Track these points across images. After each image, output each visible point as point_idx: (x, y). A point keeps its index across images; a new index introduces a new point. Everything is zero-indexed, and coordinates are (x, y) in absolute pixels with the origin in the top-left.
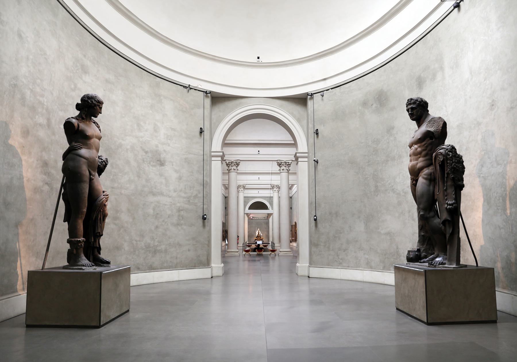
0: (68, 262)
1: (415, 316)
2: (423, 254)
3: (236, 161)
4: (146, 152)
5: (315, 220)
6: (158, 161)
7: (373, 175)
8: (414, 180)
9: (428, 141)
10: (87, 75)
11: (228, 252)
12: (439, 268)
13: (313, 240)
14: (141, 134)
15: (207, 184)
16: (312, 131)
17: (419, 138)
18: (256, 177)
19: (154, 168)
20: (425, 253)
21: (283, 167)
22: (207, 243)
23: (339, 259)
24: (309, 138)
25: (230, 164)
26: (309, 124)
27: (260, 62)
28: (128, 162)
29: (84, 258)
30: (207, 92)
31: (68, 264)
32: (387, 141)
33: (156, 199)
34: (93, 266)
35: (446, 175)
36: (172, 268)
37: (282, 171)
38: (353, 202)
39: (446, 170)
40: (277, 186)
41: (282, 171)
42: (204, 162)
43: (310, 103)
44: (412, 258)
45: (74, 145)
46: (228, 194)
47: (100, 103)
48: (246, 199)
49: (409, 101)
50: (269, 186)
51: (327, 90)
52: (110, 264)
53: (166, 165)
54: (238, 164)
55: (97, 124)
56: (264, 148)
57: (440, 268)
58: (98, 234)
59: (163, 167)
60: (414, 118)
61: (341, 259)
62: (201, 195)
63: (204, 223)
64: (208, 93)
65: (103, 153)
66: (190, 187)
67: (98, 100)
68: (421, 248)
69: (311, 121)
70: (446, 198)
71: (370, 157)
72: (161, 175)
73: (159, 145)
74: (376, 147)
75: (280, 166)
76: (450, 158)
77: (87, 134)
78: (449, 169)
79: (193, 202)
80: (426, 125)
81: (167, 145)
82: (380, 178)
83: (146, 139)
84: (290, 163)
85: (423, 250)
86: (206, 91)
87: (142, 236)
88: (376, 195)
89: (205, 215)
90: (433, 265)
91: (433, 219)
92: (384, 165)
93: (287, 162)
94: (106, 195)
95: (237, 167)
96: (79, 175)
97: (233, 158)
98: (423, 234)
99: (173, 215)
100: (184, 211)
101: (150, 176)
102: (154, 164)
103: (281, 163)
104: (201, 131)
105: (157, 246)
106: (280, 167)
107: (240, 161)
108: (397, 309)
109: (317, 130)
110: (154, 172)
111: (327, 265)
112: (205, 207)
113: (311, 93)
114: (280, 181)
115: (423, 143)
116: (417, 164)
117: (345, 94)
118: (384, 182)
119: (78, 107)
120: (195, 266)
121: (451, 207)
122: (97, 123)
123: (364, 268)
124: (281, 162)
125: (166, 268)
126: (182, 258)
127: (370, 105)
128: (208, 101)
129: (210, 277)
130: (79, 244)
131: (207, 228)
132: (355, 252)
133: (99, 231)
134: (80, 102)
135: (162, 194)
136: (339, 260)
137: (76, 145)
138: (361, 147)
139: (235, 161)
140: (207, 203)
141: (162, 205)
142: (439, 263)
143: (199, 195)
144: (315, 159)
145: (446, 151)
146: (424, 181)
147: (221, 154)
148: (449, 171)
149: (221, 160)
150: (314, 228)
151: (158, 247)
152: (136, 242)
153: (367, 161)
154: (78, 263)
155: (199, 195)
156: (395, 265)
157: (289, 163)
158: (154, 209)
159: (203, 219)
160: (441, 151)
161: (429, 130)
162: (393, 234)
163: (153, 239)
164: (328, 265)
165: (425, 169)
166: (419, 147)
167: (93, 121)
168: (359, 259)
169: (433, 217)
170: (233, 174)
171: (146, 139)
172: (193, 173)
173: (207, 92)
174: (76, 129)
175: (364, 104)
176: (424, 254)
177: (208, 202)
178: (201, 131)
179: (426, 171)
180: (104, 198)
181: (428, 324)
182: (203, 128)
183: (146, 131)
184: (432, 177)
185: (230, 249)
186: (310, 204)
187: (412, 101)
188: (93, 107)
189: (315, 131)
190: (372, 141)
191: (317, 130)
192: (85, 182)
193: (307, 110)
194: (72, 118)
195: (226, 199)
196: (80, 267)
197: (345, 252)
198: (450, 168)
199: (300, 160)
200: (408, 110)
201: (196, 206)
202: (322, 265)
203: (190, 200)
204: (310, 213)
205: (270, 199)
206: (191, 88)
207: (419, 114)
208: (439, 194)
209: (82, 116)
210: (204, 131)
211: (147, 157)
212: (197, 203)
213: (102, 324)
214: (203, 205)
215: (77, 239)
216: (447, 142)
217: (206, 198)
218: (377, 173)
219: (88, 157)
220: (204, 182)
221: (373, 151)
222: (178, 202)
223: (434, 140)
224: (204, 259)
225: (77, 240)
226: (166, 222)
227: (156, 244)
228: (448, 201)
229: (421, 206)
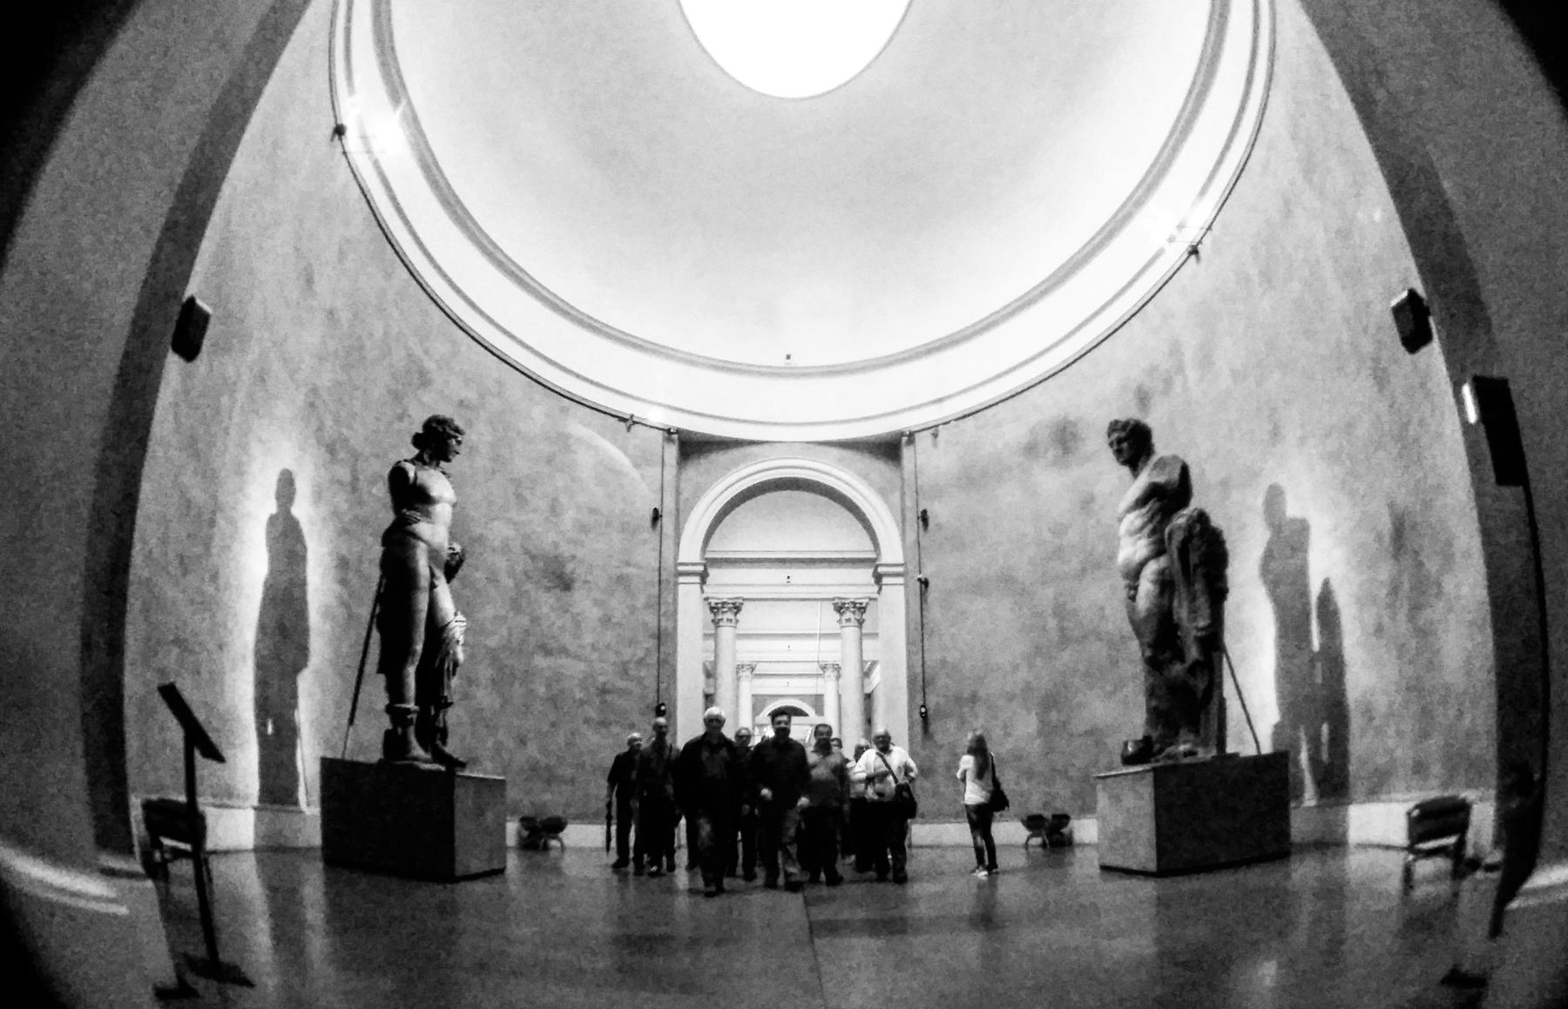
2: (1157, 747)
4: (533, 558)
9: (1152, 505)
16: (912, 516)
18: (781, 644)
21: (848, 615)
28: (493, 579)
37: (844, 623)
43: (907, 452)
50: (814, 669)
54: (737, 609)
62: (653, 660)
84: (864, 605)
87: (523, 742)
95: (736, 614)
97: (726, 594)
104: (656, 517)
106: (841, 614)
112: (663, 686)
116: (1136, 552)
128: (672, 452)
134: (421, 432)
135: (564, 651)
144: (920, 576)
147: (701, 568)
158: (548, 686)
163: (544, 750)
169: (1171, 661)
170: (726, 632)
178: (656, 517)
183: (535, 511)
186: (911, 680)
187: (1119, 426)
194: (406, 461)
199: (885, 580)
200: (1111, 444)
204: (911, 699)
206: (635, 423)
208: (1182, 612)
216: (1195, 503)
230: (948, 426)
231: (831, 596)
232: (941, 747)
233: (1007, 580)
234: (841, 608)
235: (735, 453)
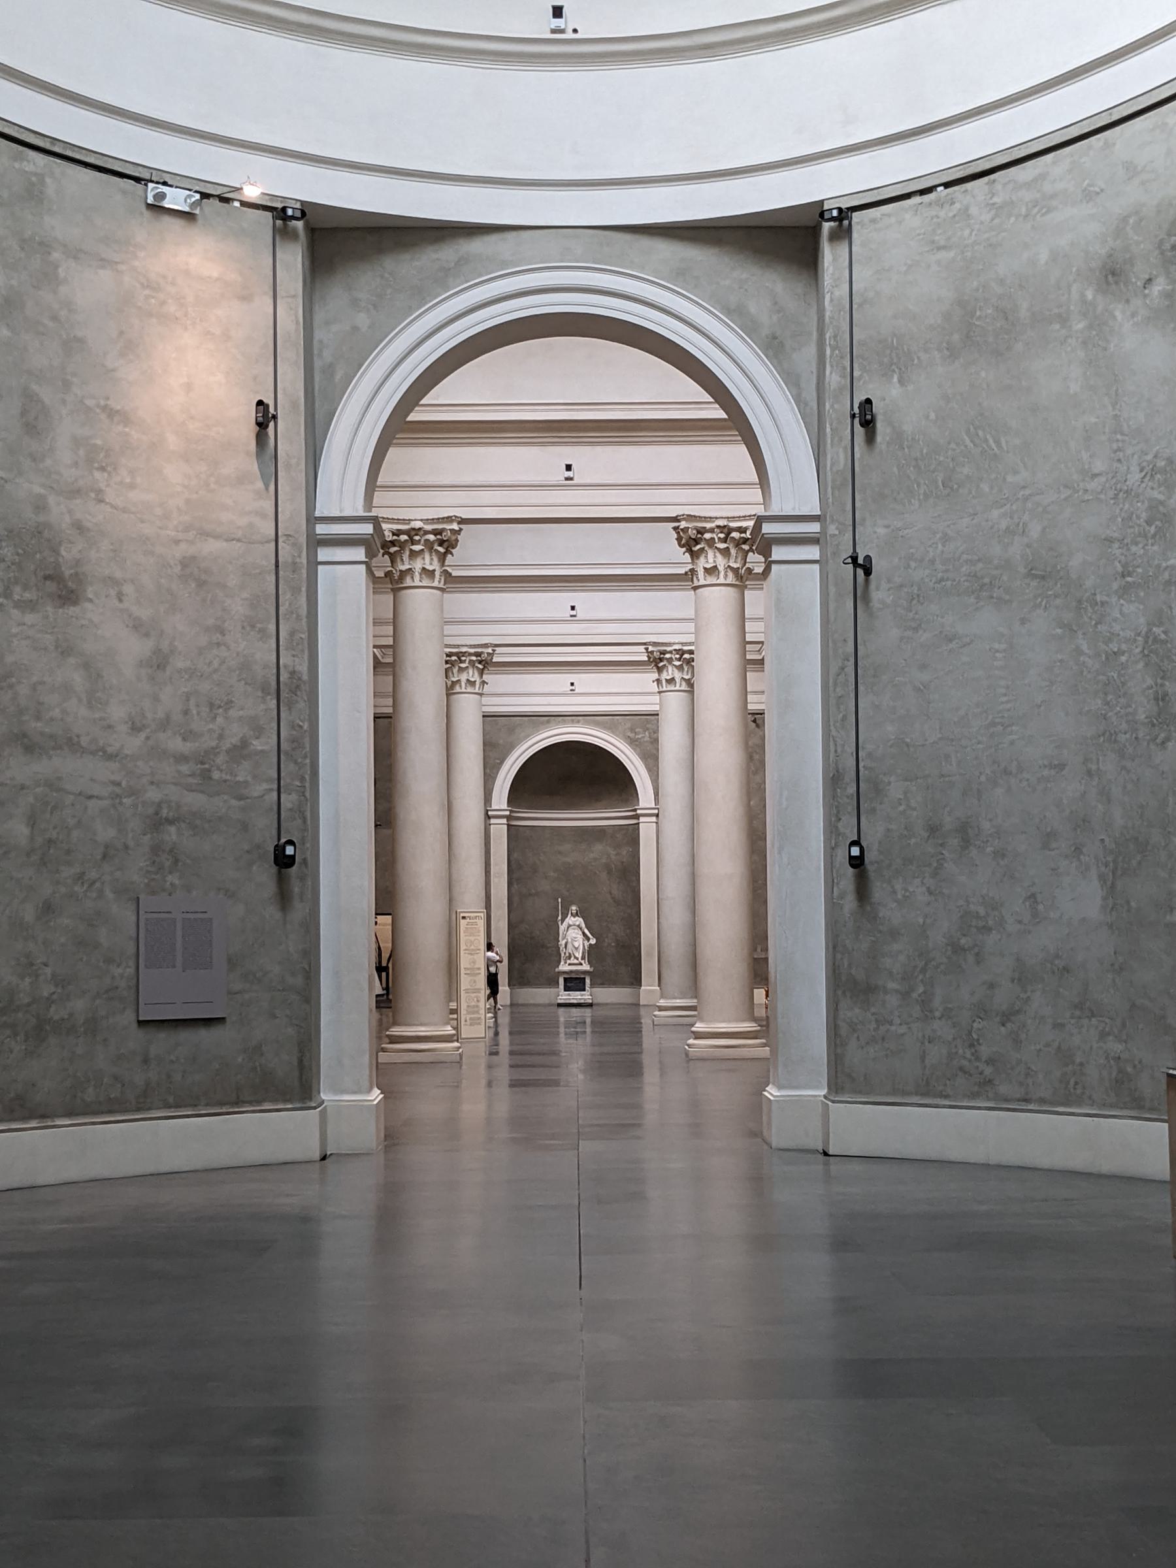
3: (440, 526)
5: (852, 866)
6: (47, 578)
7: (1146, 642)
11: (394, 1040)
15: (298, 687)
16: (839, 409)
18: (556, 602)
19: (30, 618)
21: (711, 558)
22: (299, 981)
23: (978, 1059)
25: (402, 545)
26: (828, 372)
27: (569, 35)
33: (42, 767)
38: (1046, 772)
40: (681, 652)
41: (702, 579)
42: (281, 573)
43: (831, 256)
51: (923, 192)
53: (91, 601)
54: (446, 544)
56: (599, 449)
59: (72, 610)
61: (990, 1061)
64: (293, 218)
66: (211, 705)
71: (1134, 549)
72: (65, 650)
73: (52, 500)
74: (1161, 497)
75: (690, 551)
84: (748, 535)
86: (284, 209)
89: (291, 842)
93: (686, 648)
95: (442, 558)
99: (126, 847)
100: (183, 825)
102: (27, 595)
103: (701, 531)
105: (49, 1001)
106: (694, 555)
107: (459, 523)
109: (868, 401)
111: (917, 1094)
112: (288, 801)
113: (840, 210)
114: (691, 627)
117: (1013, 219)
123: (1104, 1105)
128: (294, 258)
129: (317, 1155)
131: (299, 910)
132: (1059, 1026)
135: (72, 744)
139: (429, 527)
149: (364, 559)
150: (850, 903)
153: (1120, 569)
156: (1167, 1071)
157: (742, 530)
158: (32, 820)
159: (276, 862)
164: (925, 1094)
168: (1078, 1060)
173: (290, 212)
175: (1106, 276)
177: (302, 779)
182: (269, 401)
186: (833, 780)
189: (856, 410)
190: (1141, 471)
191: (868, 401)
197: (1009, 1025)
201: (240, 798)
202: (894, 1092)
210: (274, 417)
212: (246, 782)
214: (275, 794)
218: (1165, 632)
221: (1149, 522)
224: (281, 1063)
227: (46, 991)
230: (931, 196)
231: (672, 512)
234: (697, 541)
235: (448, 253)
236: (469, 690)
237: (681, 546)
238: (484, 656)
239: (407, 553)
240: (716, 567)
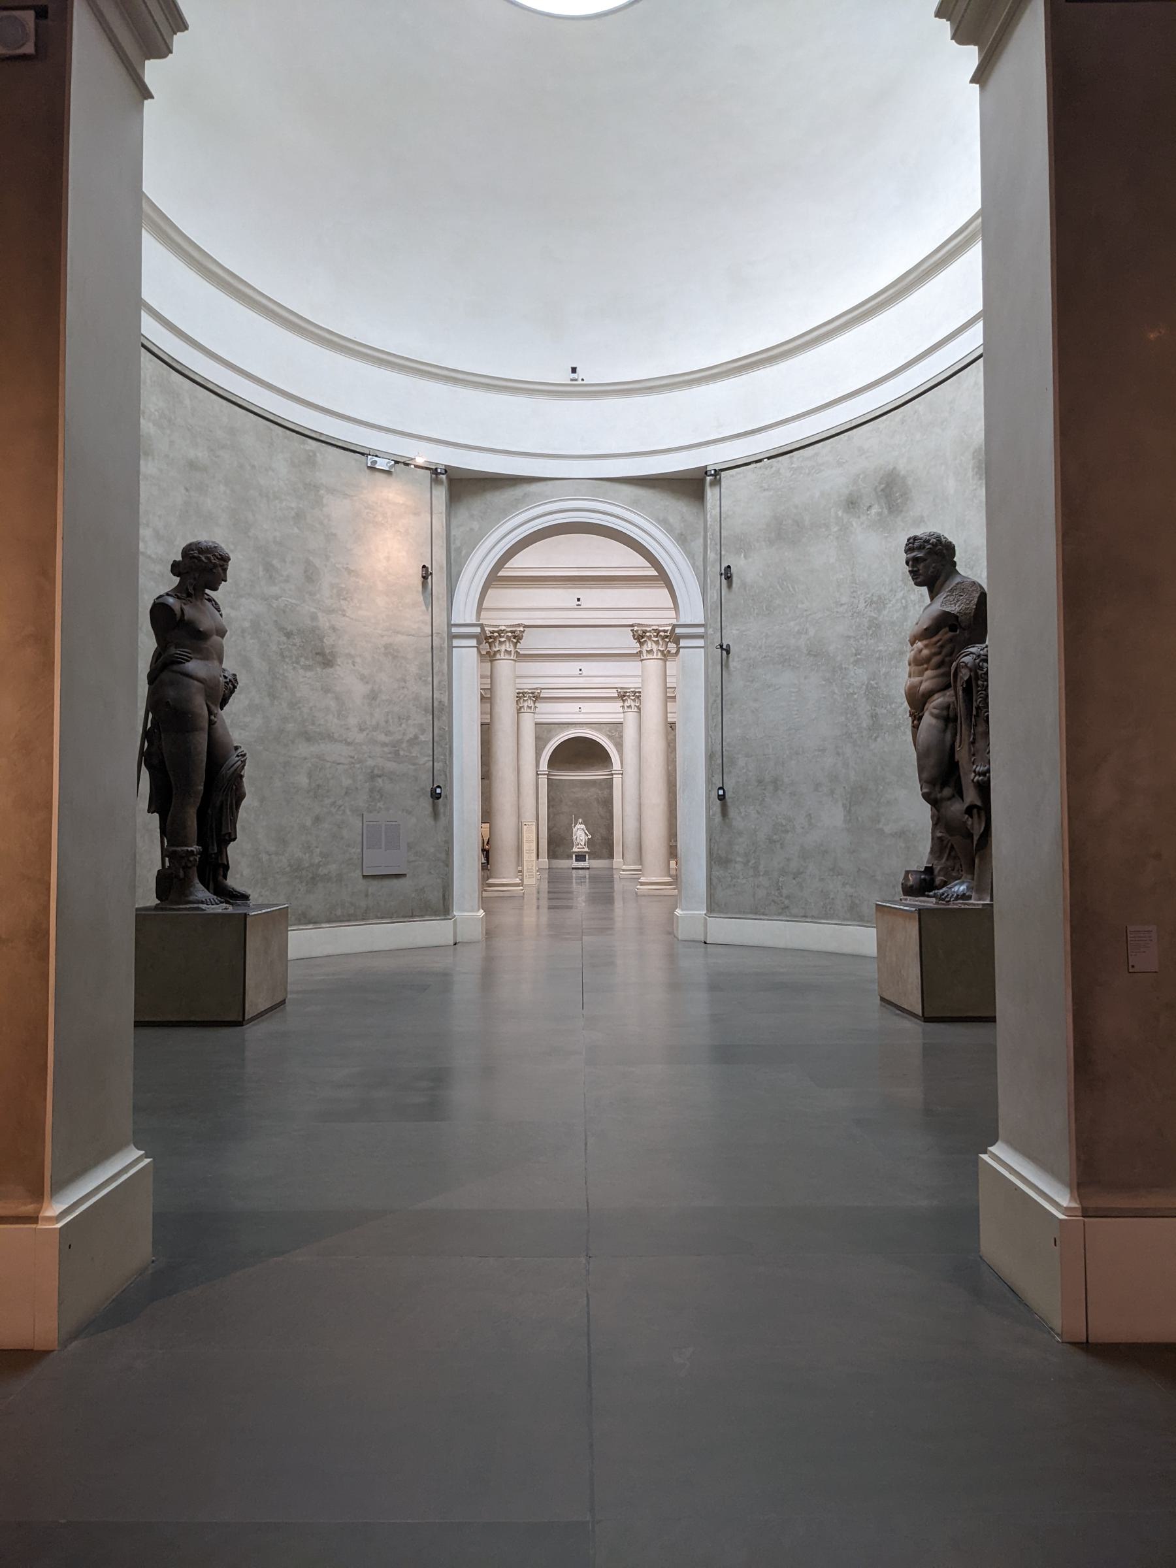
0: (157, 897)
1: (905, 1006)
4: (289, 635)
6: (317, 654)
8: (915, 716)
9: (945, 635)
10: (150, 458)
12: (955, 906)
13: (716, 847)
14: (275, 590)
15: (443, 709)
16: (714, 571)
17: (925, 627)
18: (572, 667)
19: (309, 674)
20: (944, 876)
21: (650, 645)
22: (443, 856)
23: (782, 896)
24: (707, 589)
25: (495, 638)
27: (580, 382)
29: (200, 886)
30: (439, 471)
31: (159, 902)
32: (902, 603)
33: (314, 749)
34: (222, 902)
35: (974, 712)
36: (357, 920)
39: (974, 700)
41: (645, 656)
42: (434, 652)
43: (711, 494)
44: (912, 886)
45: (174, 652)
46: (489, 716)
47: (225, 559)
48: (543, 731)
49: (910, 543)
51: (757, 462)
52: (249, 900)
54: (517, 638)
55: (216, 604)
57: (960, 904)
58: (227, 838)
59: (330, 670)
60: (919, 580)
61: (788, 897)
62: (426, 737)
63: (435, 806)
64: (441, 473)
65: (230, 665)
66: (399, 718)
67: (220, 555)
68: (934, 866)
69: (713, 542)
70: (973, 759)
71: (861, 641)
72: (326, 690)
73: (320, 614)
74: (875, 616)
75: (639, 642)
76: (983, 676)
77: (201, 629)
78: (980, 699)
79: (408, 754)
80: (942, 598)
81: (340, 612)
82: (883, 694)
83: (287, 601)
85: (940, 871)
86: (436, 469)
88: (873, 737)
89: (439, 787)
90: (943, 900)
91: (949, 803)
92: (893, 662)
93: (661, 629)
94: (242, 755)
95: (515, 645)
96: (190, 716)
98: (939, 835)
99: (357, 789)
100: (385, 778)
101: (298, 695)
102: (307, 663)
103: (645, 632)
105: (319, 865)
106: (641, 644)
107: (524, 627)
108: (882, 999)
110: (308, 684)
113: (715, 470)
115: (935, 639)
116: (921, 683)
117: (802, 475)
118: (893, 706)
119: (176, 568)
120: (412, 916)
121: (981, 778)
122: (214, 601)
123: (844, 919)
124: (644, 629)
125: (341, 921)
126: (379, 896)
127: (865, 508)
128: (441, 493)
130: (192, 859)
131: (443, 821)
132: (822, 880)
133: (230, 831)
134: (179, 558)
135: (329, 737)
136: (781, 898)
137: (179, 652)
138: (838, 616)
139: (530, 691)
140: (442, 757)
141: (328, 765)
142: (958, 895)
143: (421, 737)
145: (975, 659)
146: (934, 721)
148: (980, 702)
150: (718, 818)
151: (321, 868)
152: (268, 857)
153: (854, 651)
154: (187, 896)
155: (422, 738)
157: (665, 631)
158: (310, 776)
160: (967, 659)
161: (948, 609)
162: (913, 834)
165: (936, 696)
166: (926, 646)
167: (207, 597)
168: (831, 897)
170: (505, 667)
171: (286, 603)
172: (406, 683)
173: (439, 471)
174: (178, 619)
176: (942, 878)
177: (445, 755)
179: (938, 700)
180: (238, 761)
181: (927, 1019)
183: (287, 581)
184: (951, 714)
185: (495, 878)
186: (710, 757)
187: (917, 544)
188: (211, 569)
189: (723, 572)
190: (865, 602)
192: (202, 729)
193: (704, 512)
195: (487, 730)
196: (196, 905)
198: (982, 695)
200: (907, 563)
201: (414, 764)
202: (740, 912)
203: (398, 750)
204: (709, 781)
205: (615, 730)
207: (929, 573)
209: (187, 589)
210: (431, 574)
211: (290, 646)
213: (247, 1017)
214: (431, 763)
215: (186, 848)
217: (442, 744)
218: (876, 683)
219: (204, 677)
220: (435, 705)
222: (370, 757)
223: (958, 632)
224: (434, 897)
225: (187, 850)
226: (340, 807)
227: (317, 860)
228: (977, 766)
229: (925, 775)
231: (630, 622)
232: (740, 834)
233: (817, 653)
236: (507, 657)
237: (635, 639)
238: (536, 694)
239: (498, 642)
240: (652, 650)
